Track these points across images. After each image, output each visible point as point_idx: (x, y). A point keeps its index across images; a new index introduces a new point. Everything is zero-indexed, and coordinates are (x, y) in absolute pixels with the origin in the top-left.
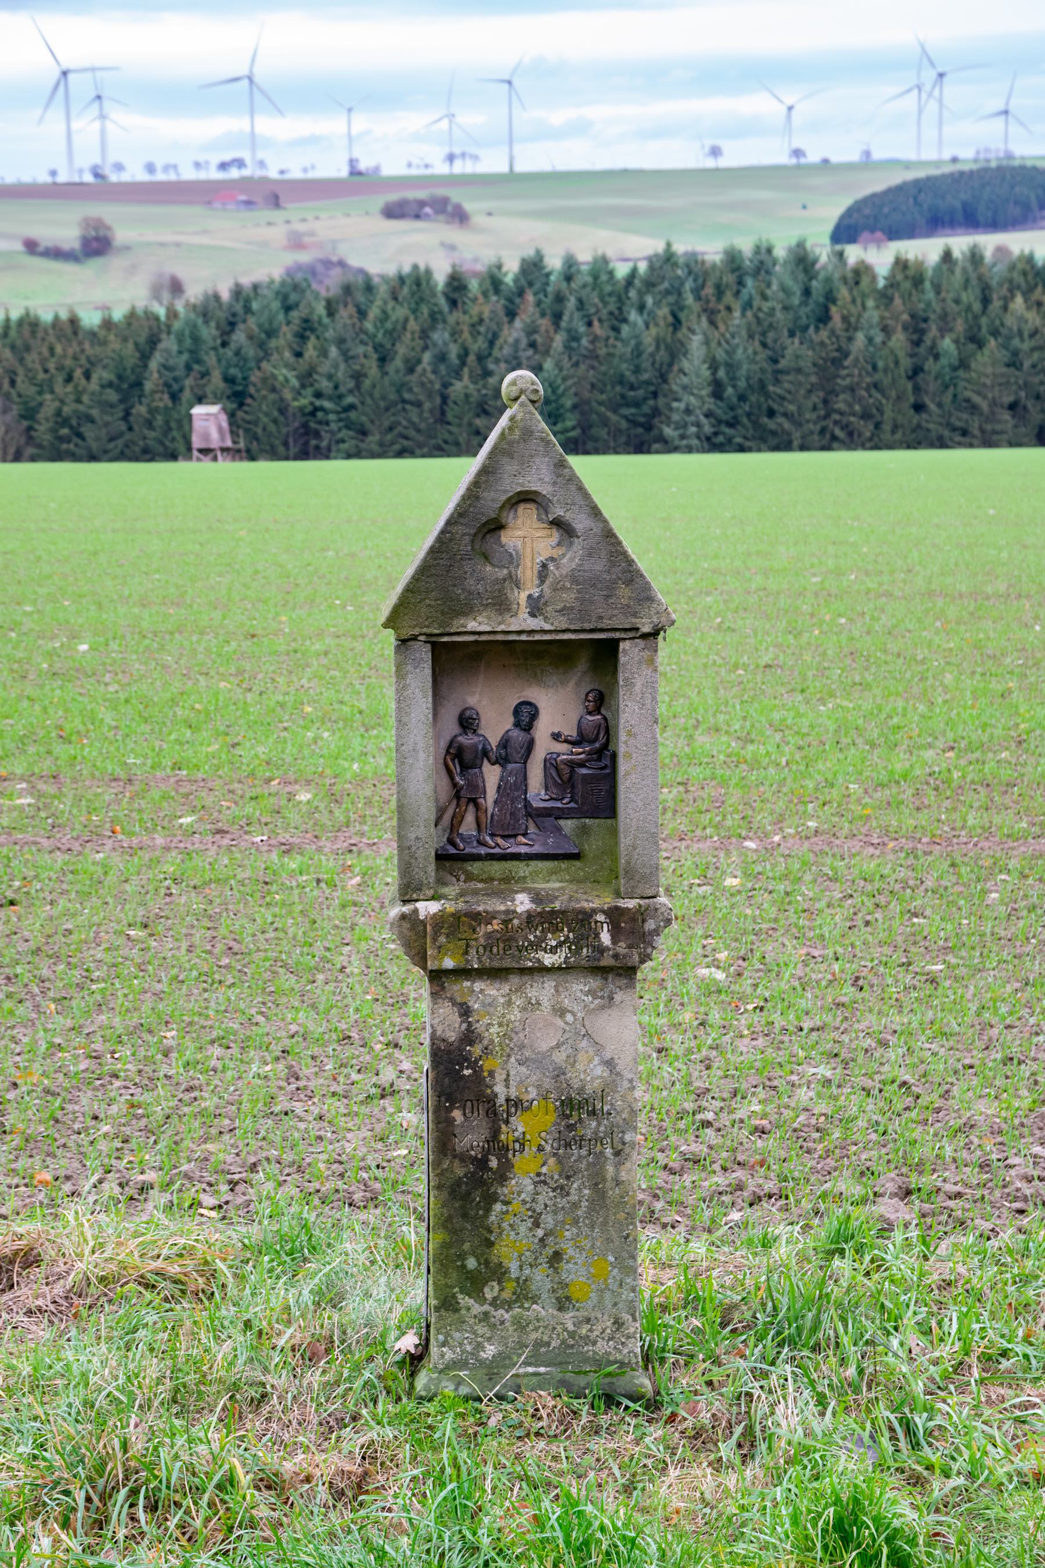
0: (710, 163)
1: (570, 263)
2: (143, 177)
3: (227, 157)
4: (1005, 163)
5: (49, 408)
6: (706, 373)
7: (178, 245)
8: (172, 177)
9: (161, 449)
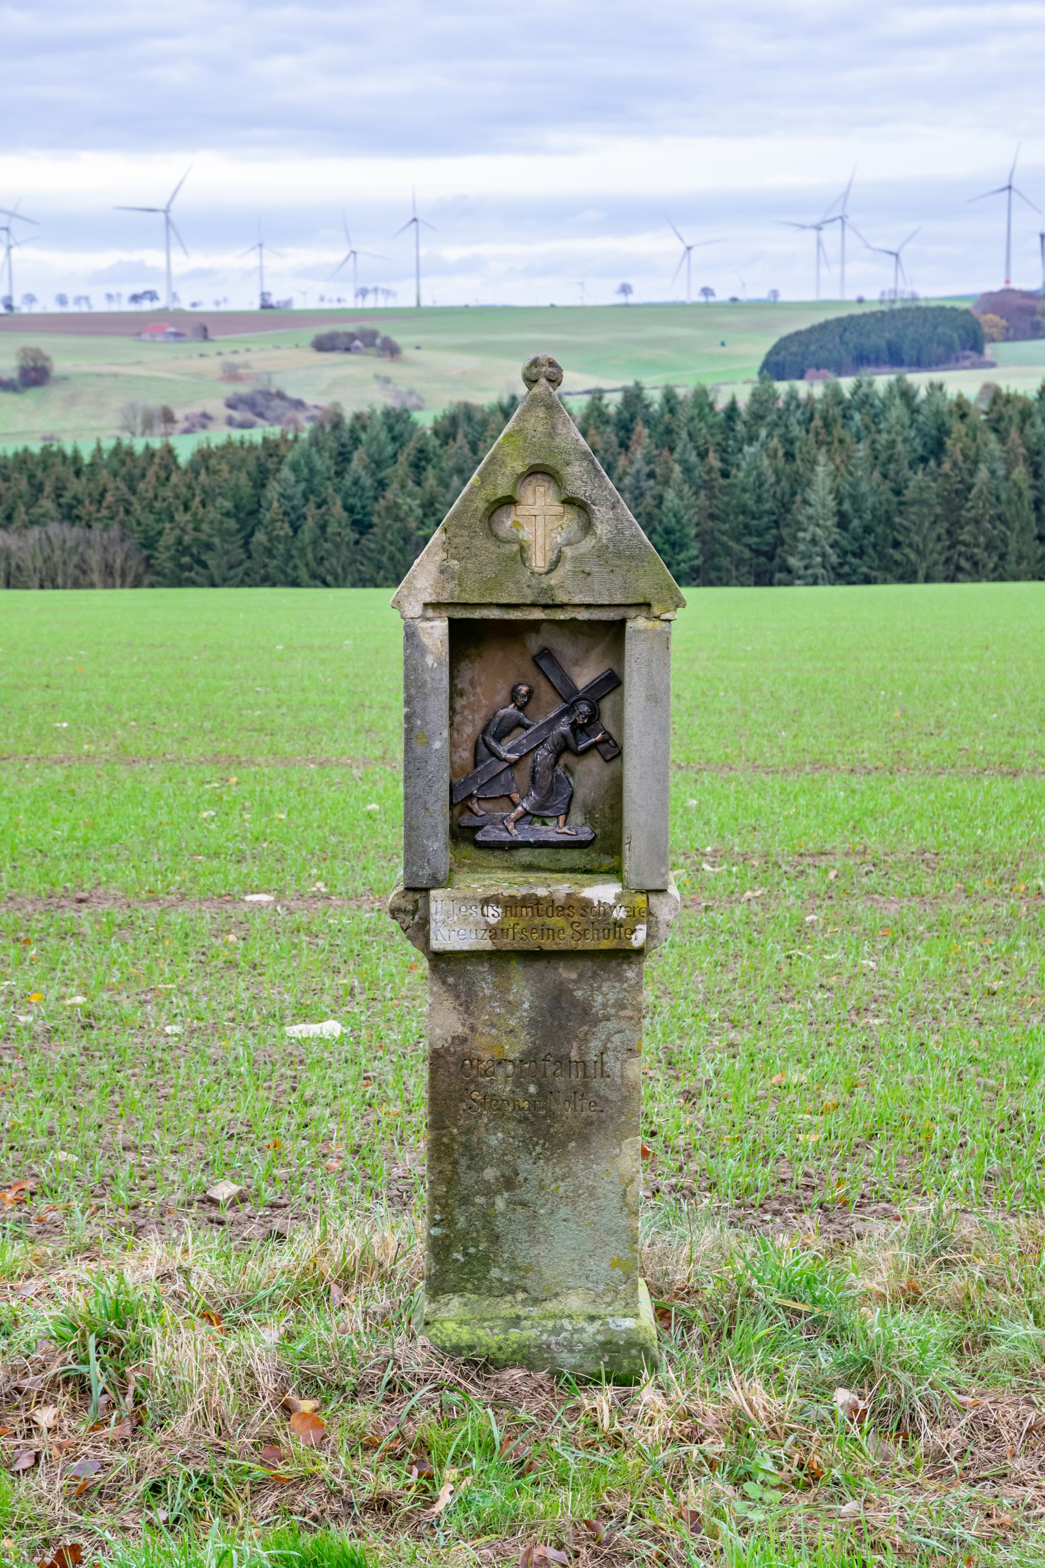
0: (621, 299)
1: (669, 397)
2: (54, 308)
3: (139, 289)
4: (909, 304)
5: (169, 538)
6: (832, 504)
7: (115, 376)
8: (84, 308)
9: (282, 577)
